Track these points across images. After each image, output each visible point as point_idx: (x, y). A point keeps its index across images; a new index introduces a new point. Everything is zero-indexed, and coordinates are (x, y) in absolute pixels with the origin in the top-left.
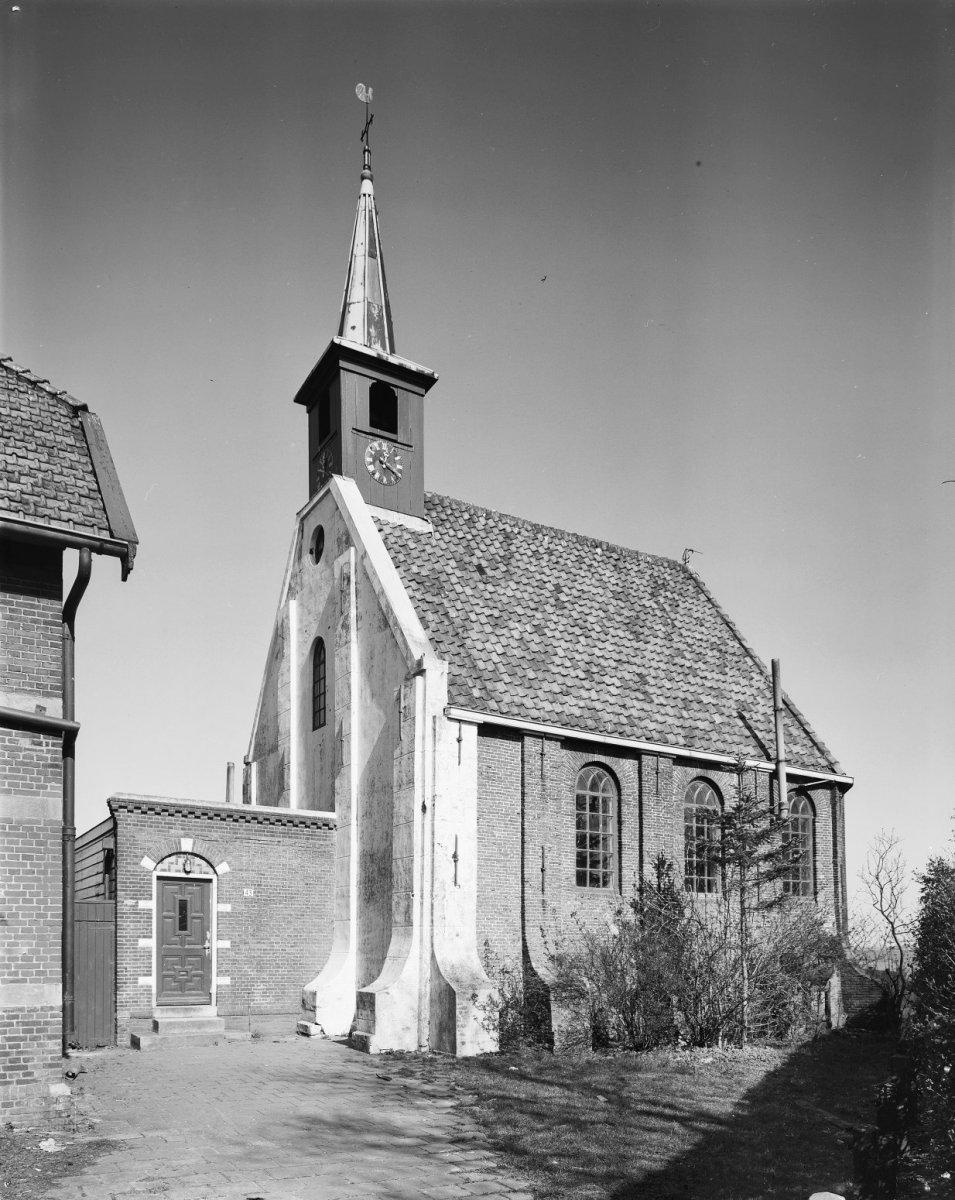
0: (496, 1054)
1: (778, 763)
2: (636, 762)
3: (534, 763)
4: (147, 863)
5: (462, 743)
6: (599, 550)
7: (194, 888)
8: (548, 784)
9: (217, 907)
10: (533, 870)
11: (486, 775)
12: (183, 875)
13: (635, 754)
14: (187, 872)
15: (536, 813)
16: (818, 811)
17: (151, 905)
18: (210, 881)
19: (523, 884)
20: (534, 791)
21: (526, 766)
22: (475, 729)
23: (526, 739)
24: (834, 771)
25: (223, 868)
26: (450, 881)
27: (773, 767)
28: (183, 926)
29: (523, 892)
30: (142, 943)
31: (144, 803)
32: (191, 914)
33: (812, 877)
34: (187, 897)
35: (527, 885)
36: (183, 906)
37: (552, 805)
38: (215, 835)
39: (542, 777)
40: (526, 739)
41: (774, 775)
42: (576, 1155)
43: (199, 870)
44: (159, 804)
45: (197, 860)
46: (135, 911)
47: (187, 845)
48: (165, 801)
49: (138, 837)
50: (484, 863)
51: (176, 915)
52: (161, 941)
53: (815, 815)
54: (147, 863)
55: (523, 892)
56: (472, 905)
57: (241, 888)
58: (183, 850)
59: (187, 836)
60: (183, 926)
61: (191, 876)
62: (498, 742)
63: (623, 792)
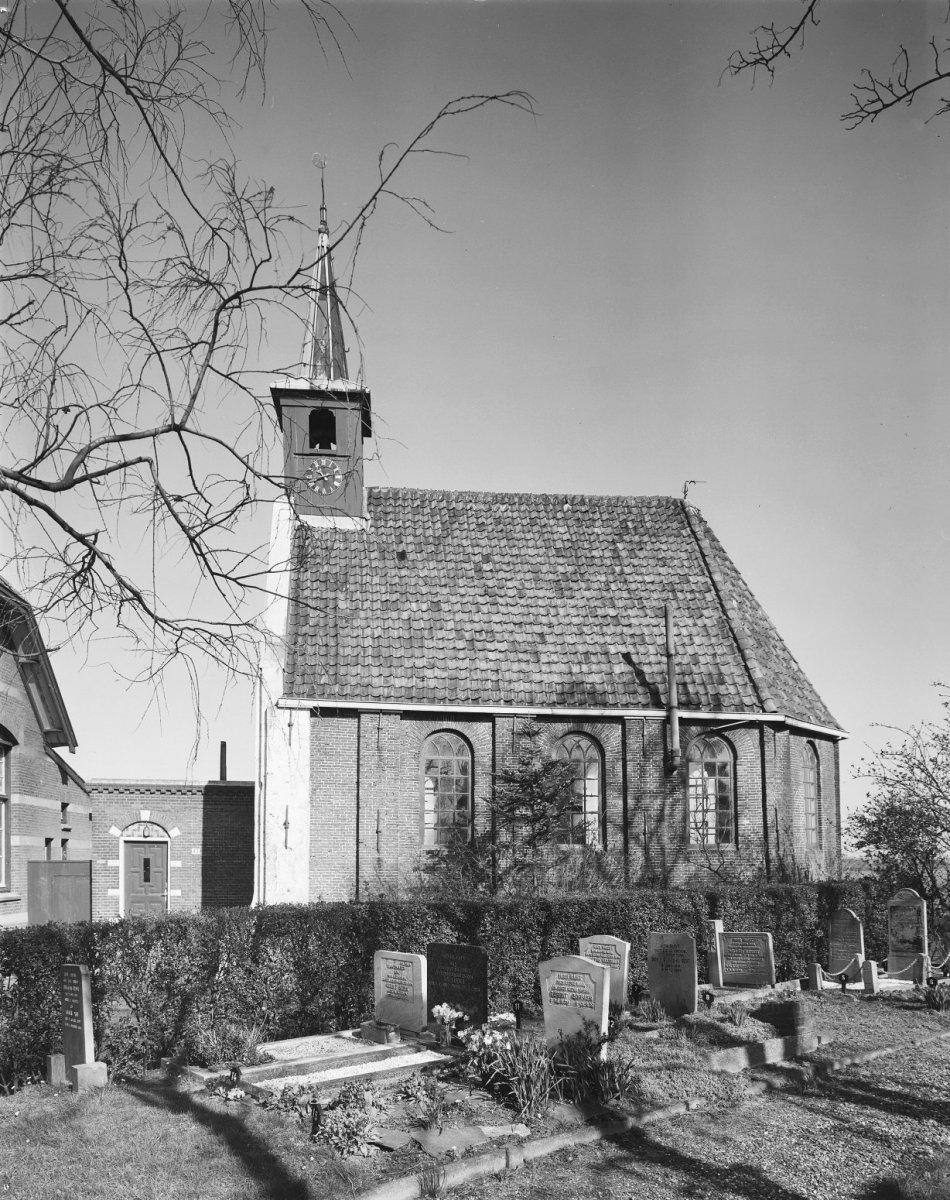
0: (862, 990)
1: (670, 709)
2: (490, 724)
3: (369, 737)
4: (115, 831)
5: (293, 728)
6: (566, 507)
7: (156, 848)
8: (386, 754)
9: (173, 864)
10: (368, 832)
11: (320, 751)
12: (142, 839)
13: (490, 718)
14: (145, 836)
15: (372, 781)
16: (740, 753)
17: (120, 863)
18: (166, 843)
19: (357, 844)
20: (370, 761)
21: (362, 739)
22: (307, 714)
23: (363, 716)
24: (764, 711)
25: (175, 832)
26: (282, 846)
27: (662, 713)
28: (147, 879)
29: (358, 851)
30: (111, 892)
31: (110, 785)
32: (153, 869)
33: (733, 824)
34: (149, 856)
35: (360, 845)
36: (147, 862)
37: (389, 773)
38: (167, 806)
39: (379, 749)
40: (363, 716)
41: (667, 720)
42: (392, 1087)
43: (156, 835)
44: (121, 786)
45: (156, 827)
46: (106, 868)
47: (145, 815)
48: (127, 783)
49: (107, 811)
50: (317, 829)
51: (141, 869)
52: (129, 889)
53: (736, 757)
54: (115, 831)
55: (358, 851)
56: (305, 863)
57: (189, 849)
58: (143, 819)
59: (146, 808)
60: (147, 879)
61: (148, 839)
62: (335, 720)
63: (476, 754)
